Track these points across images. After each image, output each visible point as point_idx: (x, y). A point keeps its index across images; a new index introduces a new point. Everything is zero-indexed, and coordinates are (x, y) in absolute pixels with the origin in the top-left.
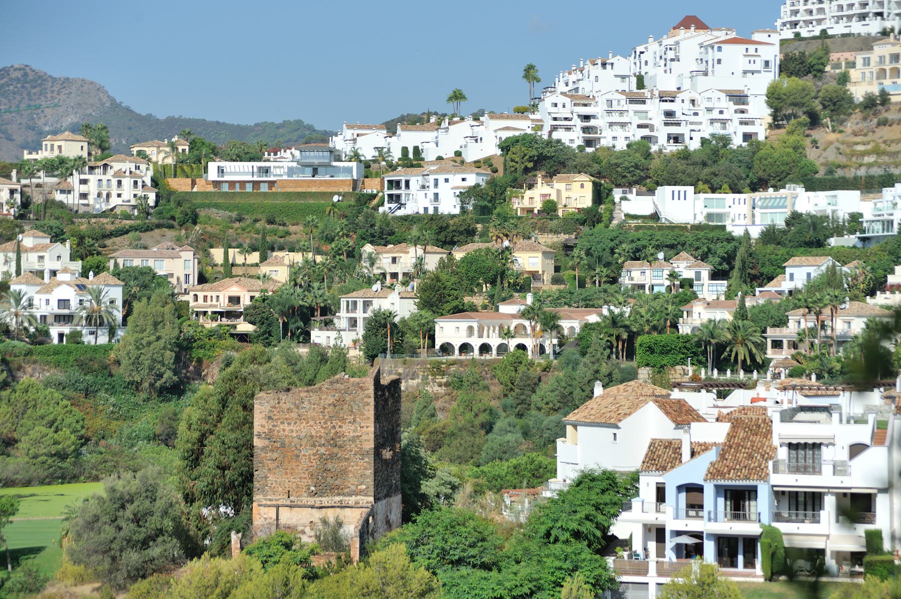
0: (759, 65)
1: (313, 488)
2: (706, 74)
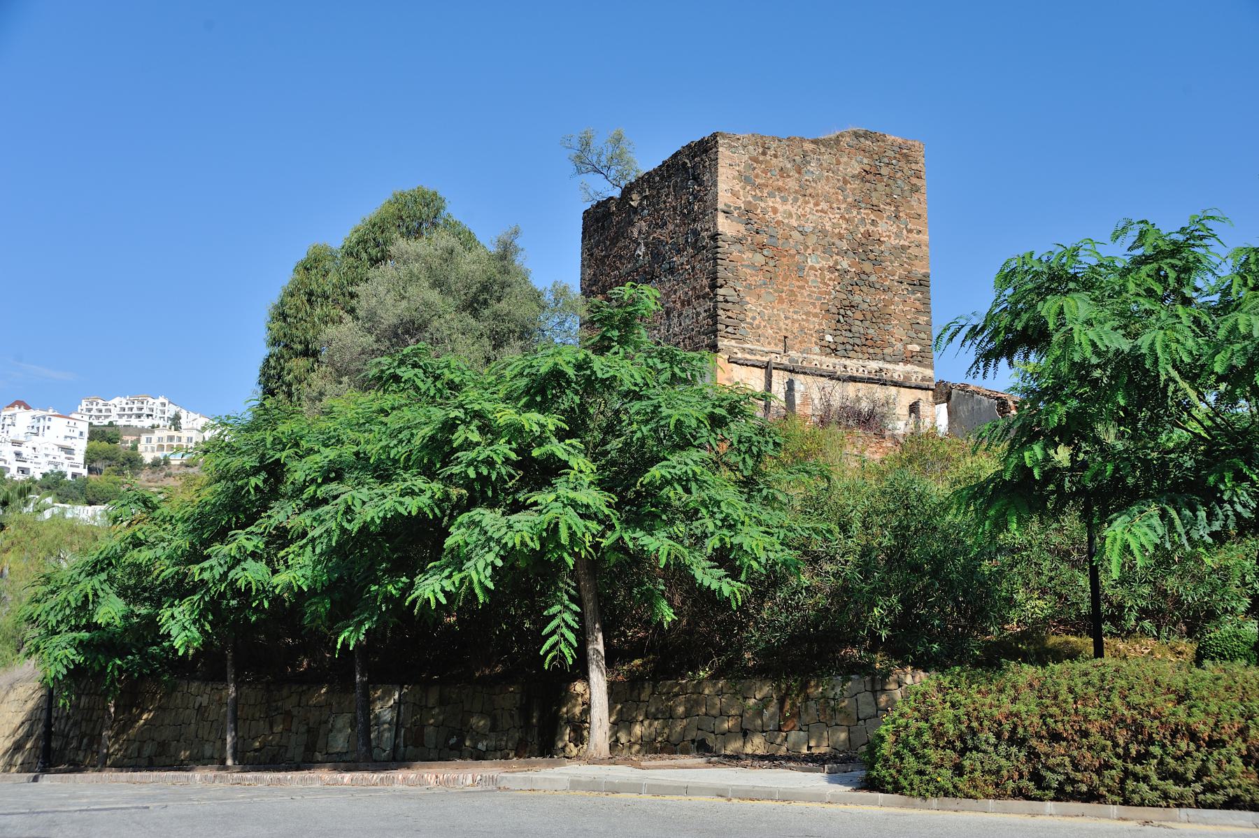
0: (77, 434)
1: (829, 338)
2: (37, 434)
